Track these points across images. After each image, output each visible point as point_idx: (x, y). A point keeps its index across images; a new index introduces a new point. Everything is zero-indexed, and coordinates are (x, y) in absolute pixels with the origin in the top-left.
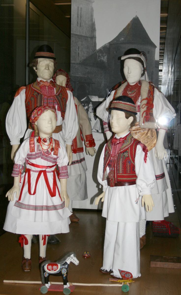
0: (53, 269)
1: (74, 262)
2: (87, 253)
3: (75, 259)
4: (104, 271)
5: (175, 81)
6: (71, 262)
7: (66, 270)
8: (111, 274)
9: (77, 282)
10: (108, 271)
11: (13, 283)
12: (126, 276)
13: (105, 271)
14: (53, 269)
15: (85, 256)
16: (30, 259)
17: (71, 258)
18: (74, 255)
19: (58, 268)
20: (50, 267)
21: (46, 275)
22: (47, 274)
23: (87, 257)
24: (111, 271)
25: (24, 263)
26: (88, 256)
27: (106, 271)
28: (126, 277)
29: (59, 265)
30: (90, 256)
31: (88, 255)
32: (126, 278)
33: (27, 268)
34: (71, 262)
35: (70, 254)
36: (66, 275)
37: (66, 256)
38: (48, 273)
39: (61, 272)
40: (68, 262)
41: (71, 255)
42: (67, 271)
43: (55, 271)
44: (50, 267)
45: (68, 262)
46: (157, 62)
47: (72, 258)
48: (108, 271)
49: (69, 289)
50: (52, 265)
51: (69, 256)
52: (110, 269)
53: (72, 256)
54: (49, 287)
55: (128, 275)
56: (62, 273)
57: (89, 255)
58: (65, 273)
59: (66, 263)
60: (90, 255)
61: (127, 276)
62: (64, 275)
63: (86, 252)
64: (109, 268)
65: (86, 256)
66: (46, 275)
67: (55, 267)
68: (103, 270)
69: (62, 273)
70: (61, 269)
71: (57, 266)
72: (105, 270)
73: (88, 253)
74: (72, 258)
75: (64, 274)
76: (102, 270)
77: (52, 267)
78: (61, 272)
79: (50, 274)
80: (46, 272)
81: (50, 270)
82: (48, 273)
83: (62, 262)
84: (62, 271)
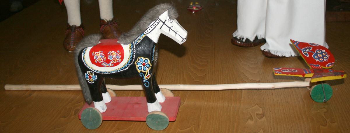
0: (108, 61)
1: (171, 35)
2: (195, 3)
3: (175, 25)
4: (242, 42)
5: (155, 20)
6: (163, 37)
7: (149, 63)
8: (263, 48)
9: (185, 83)
10: (252, 39)
11: (27, 91)
12: (316, 57)
13: (244, 40)
14: (108, 61)
15: (192, 11)
16: (82, 26)
17: (161, 23)
18: (168, 13)
19: (122, 58)
20: (100, 57)
21: (90, 77)
22: (93, 76)
23: (196, 11)
24: (261, 41)
25: (68, 36)
26: (197, 9)
27: (247, 40)
28: (317, 60)
29: (127, 49)
30: (200, 10)
31: (196, 7)
32: (318, 63)
33: (72, 47)
34: (163, 37)
35: (158, 11)
36: (150, 75)
37: (145, 20)
38: (95, 73)
39: (133, 68)
40: (154, 37)
41: (160, 14)
42: (152, 62)
43: (115, 65)
44: (99, 56)
45: (154, 37)
46: (159, 14)
47: (164, 23)
48: (252, 39)
49: (163, 114)
50: (105, 49)
51: (155, 18)
52: (255, 36)
53: (164, 16)
54: (106, 108)
55: (321, 55)
56: (138, 69)
57: (199, 8)
58: (148, 69)
59: (147, 39)
60: (201, 7)
61: (319, 58)
62: (145, 77)
63: (194, 4)
64: (254, 34)
65: (194, 10)
66: (94, 78)
67: (113, 55)
68: (241, 39)
69: (139, 71)
70: (132, 58)
71: (121, 49)
72: (243, 38)
73: (196, 3)
74: (164, 23)
75: (144, 73)
76: (236, 38)
77: (106, 56)
78: (133, 68)
79: (100, 76)
80: (89, 70)
81: (99, 65)
82: (95, 73)
83: (135, 37)
84: (137, 66)
